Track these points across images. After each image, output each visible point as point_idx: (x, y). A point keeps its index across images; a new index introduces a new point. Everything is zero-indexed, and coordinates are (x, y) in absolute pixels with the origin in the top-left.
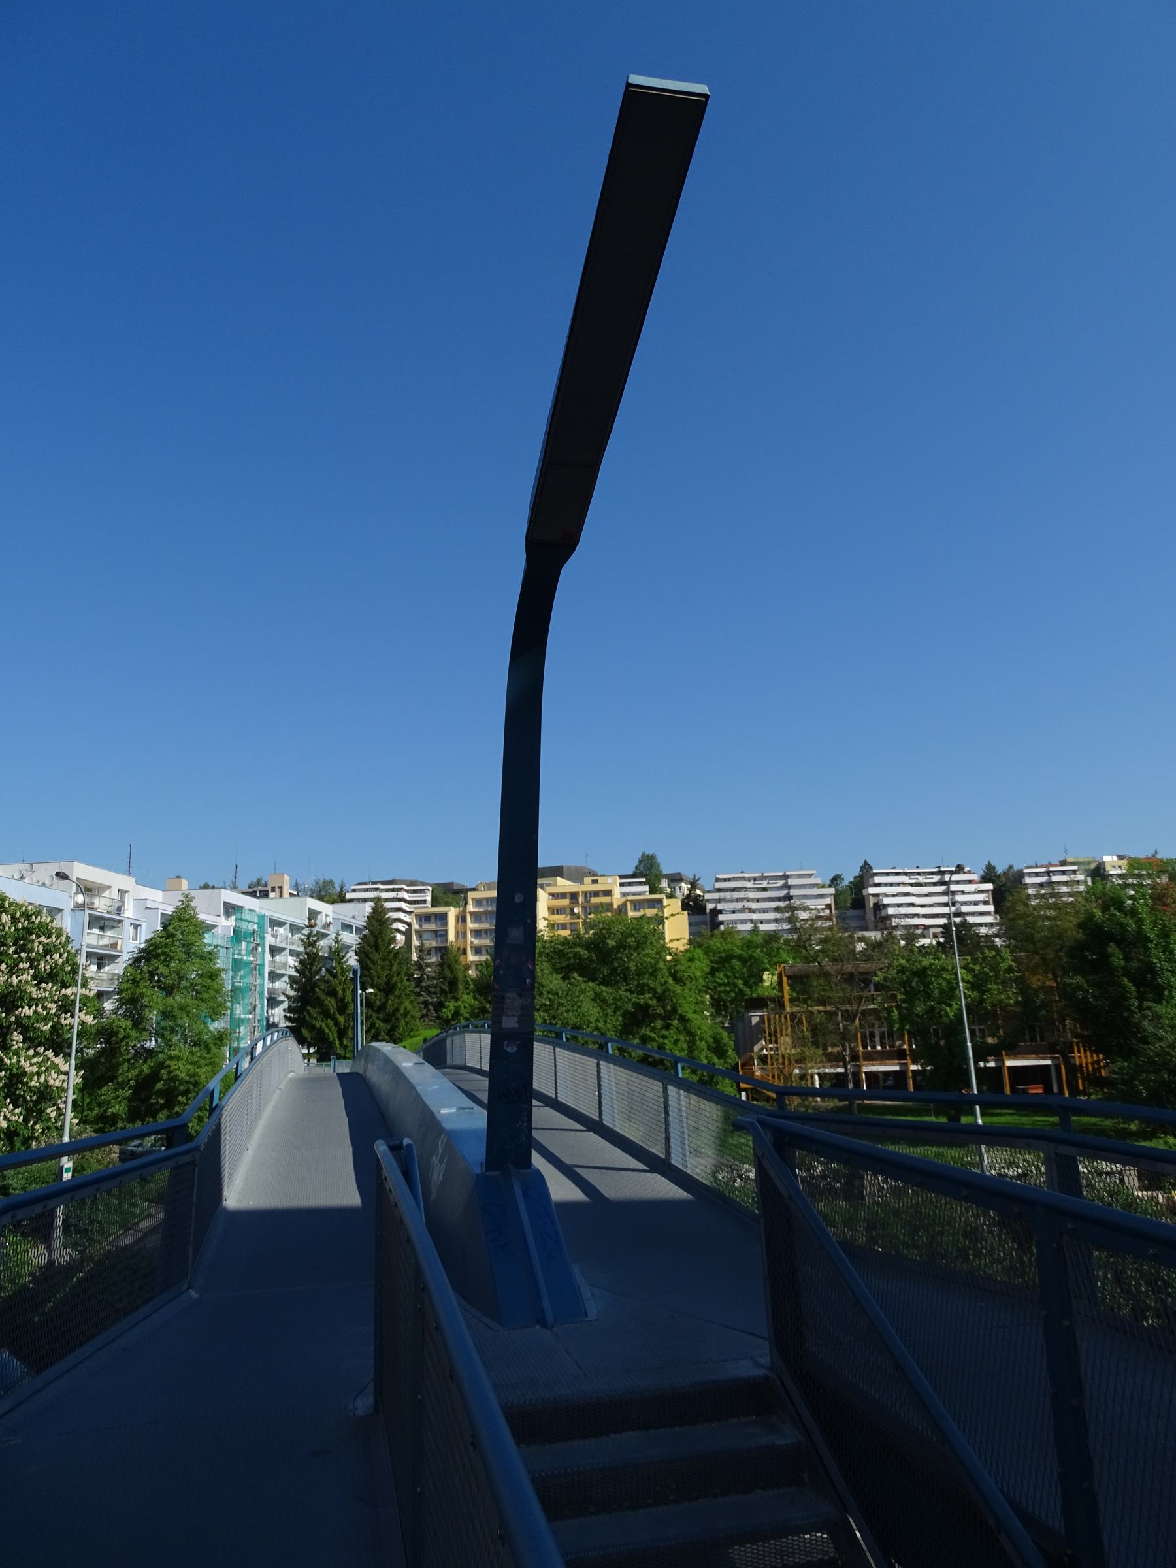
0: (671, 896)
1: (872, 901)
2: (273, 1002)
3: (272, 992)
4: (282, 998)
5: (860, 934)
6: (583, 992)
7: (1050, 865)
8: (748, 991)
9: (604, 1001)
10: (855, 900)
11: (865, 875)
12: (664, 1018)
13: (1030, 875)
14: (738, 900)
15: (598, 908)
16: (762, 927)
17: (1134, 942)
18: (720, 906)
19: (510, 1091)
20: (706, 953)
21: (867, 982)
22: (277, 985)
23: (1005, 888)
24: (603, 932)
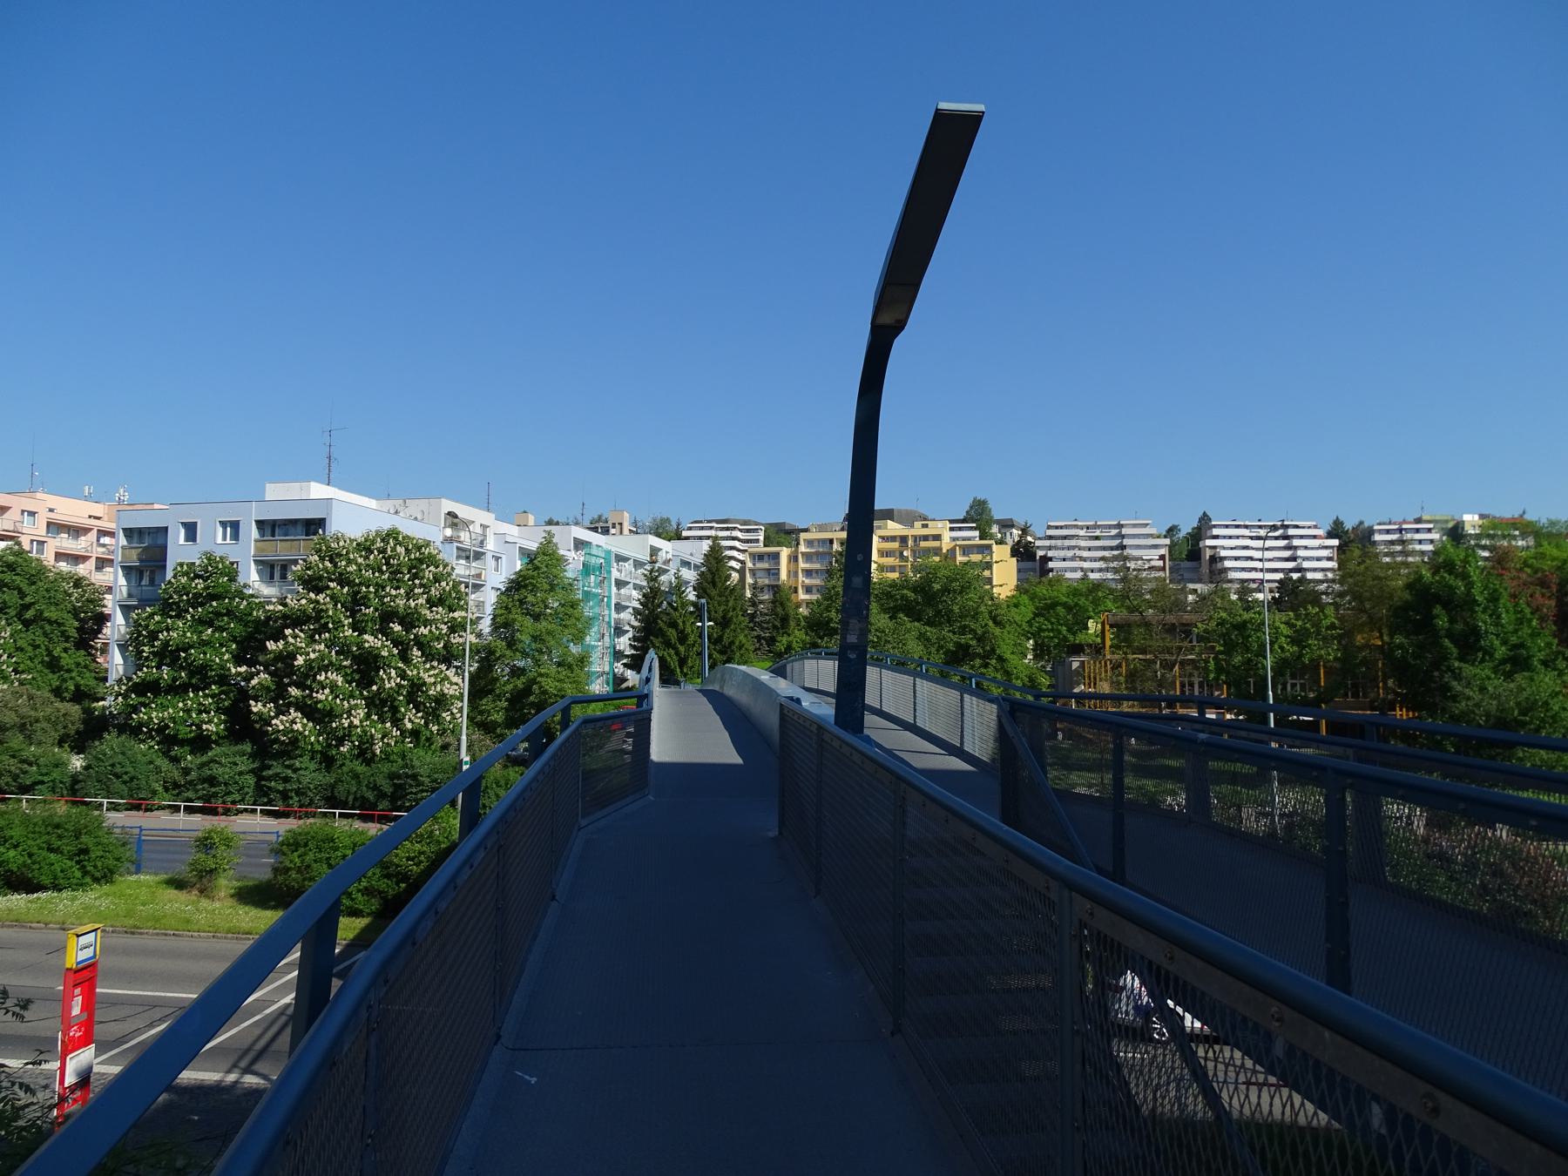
0: (1001, 542)
1: (1208, 553)
2: (619, 631)
3: (618, 622)
4: (627, 628)
5: (1191, 586)
6: (909, 631)
7: (1405, 522)
8: (1071, 638)
9: (928, 640)
10: (1191, 552)
11: (1204, 526)
12: (982, 657)
13: (1380, 532)
14: (1069, 548)
15: (927, 551)
16: (1092, 576)
17: (1459, 606)
18: (1050, 554)
19: (850, 692)
20: (1032, 599)
21: (1188, 633)
22: (622, 615)
23: (1352, 542)
24: (930, 575)
